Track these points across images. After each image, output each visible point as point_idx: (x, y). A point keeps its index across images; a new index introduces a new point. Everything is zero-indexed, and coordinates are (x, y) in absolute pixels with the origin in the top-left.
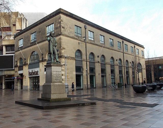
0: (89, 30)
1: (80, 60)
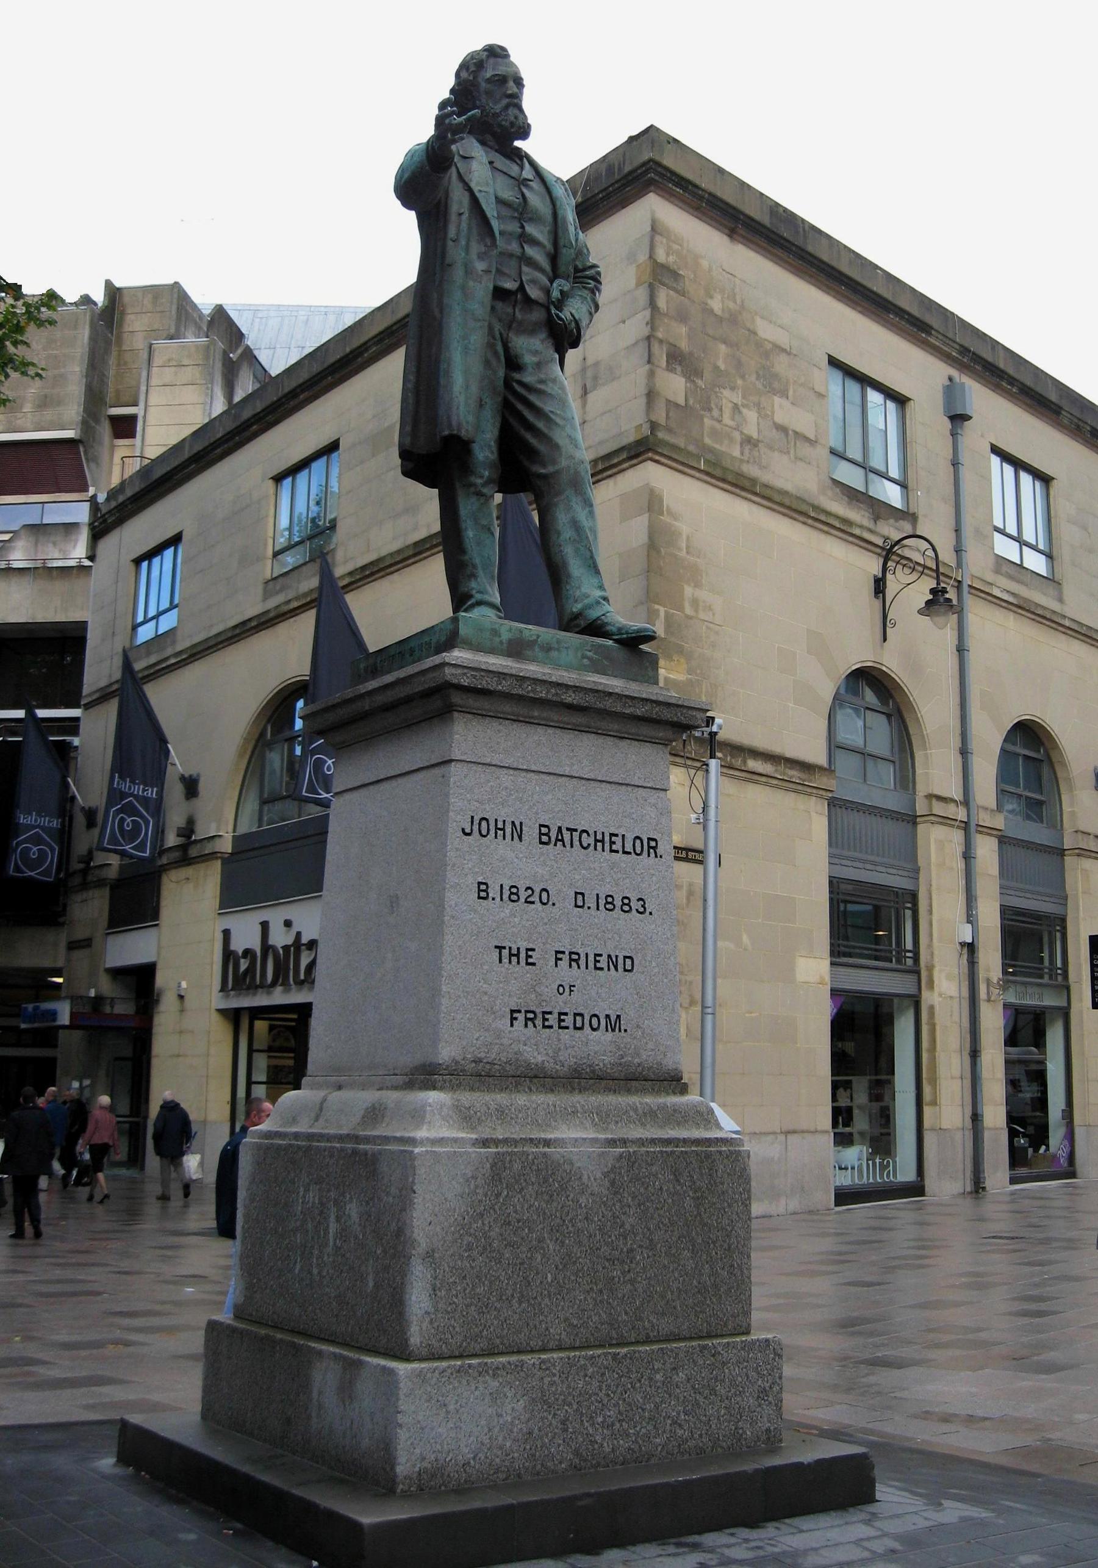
0: (995, 450)
1: (893, 802)
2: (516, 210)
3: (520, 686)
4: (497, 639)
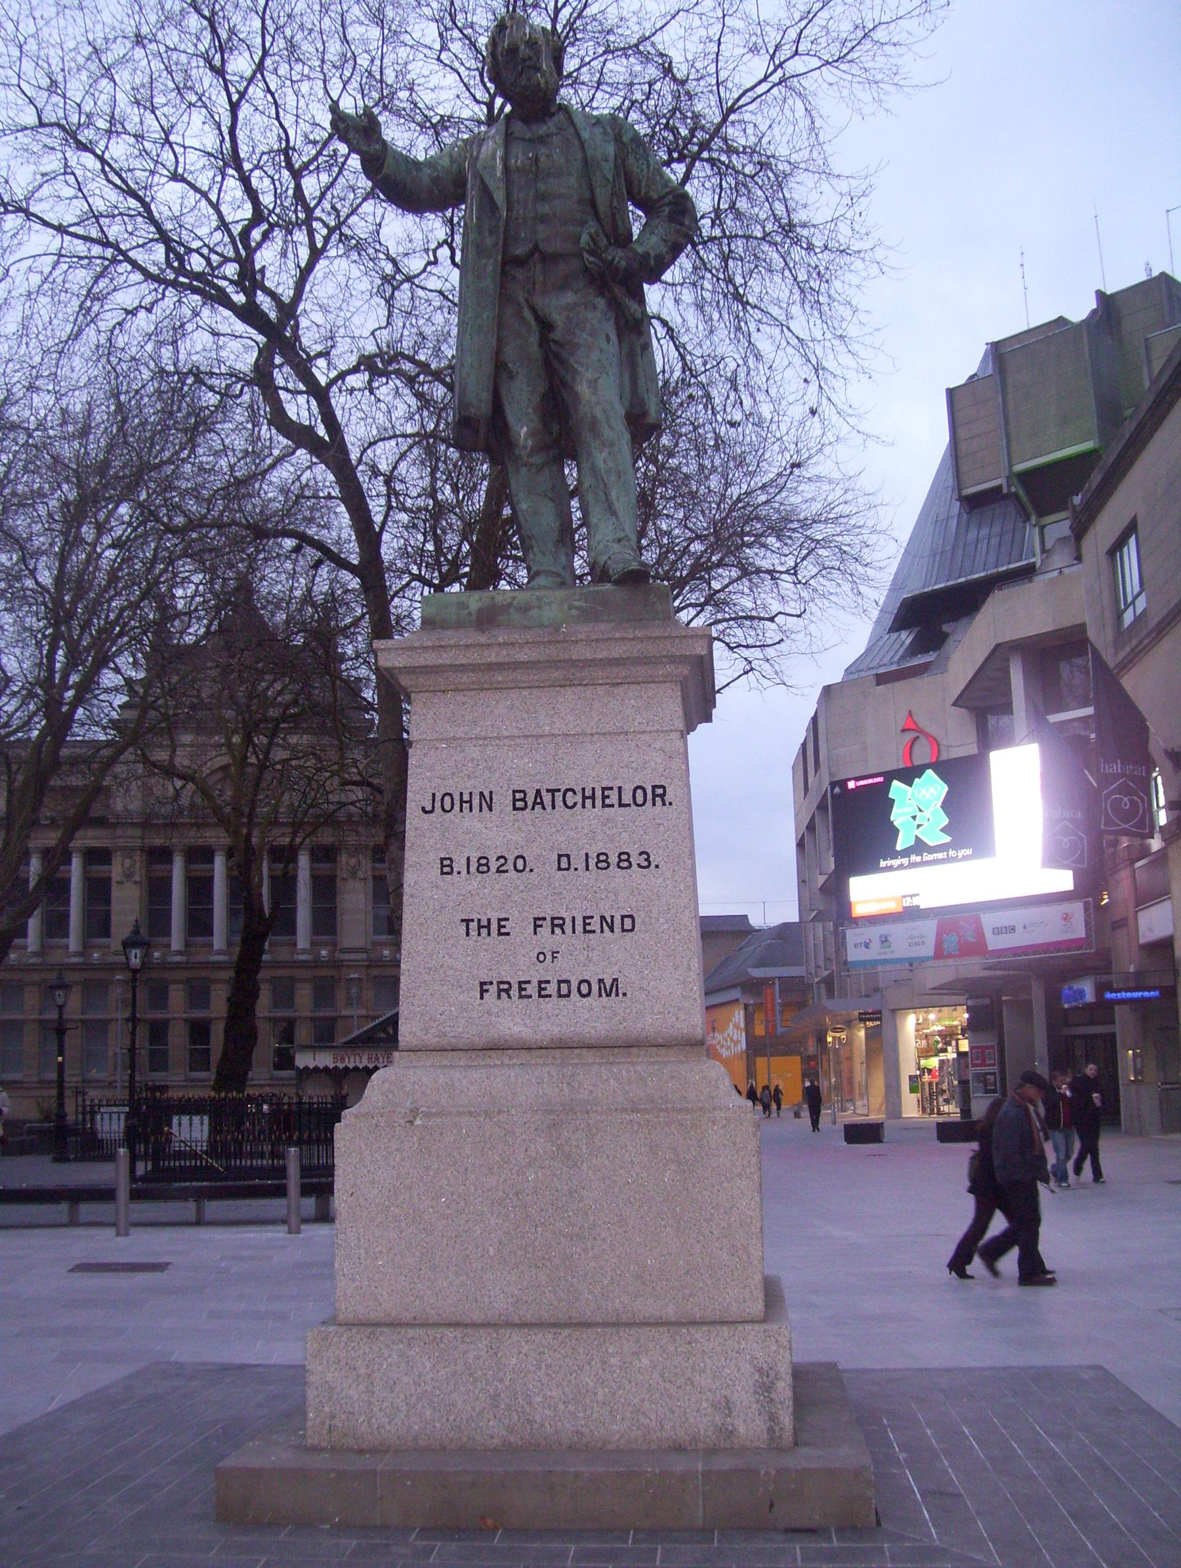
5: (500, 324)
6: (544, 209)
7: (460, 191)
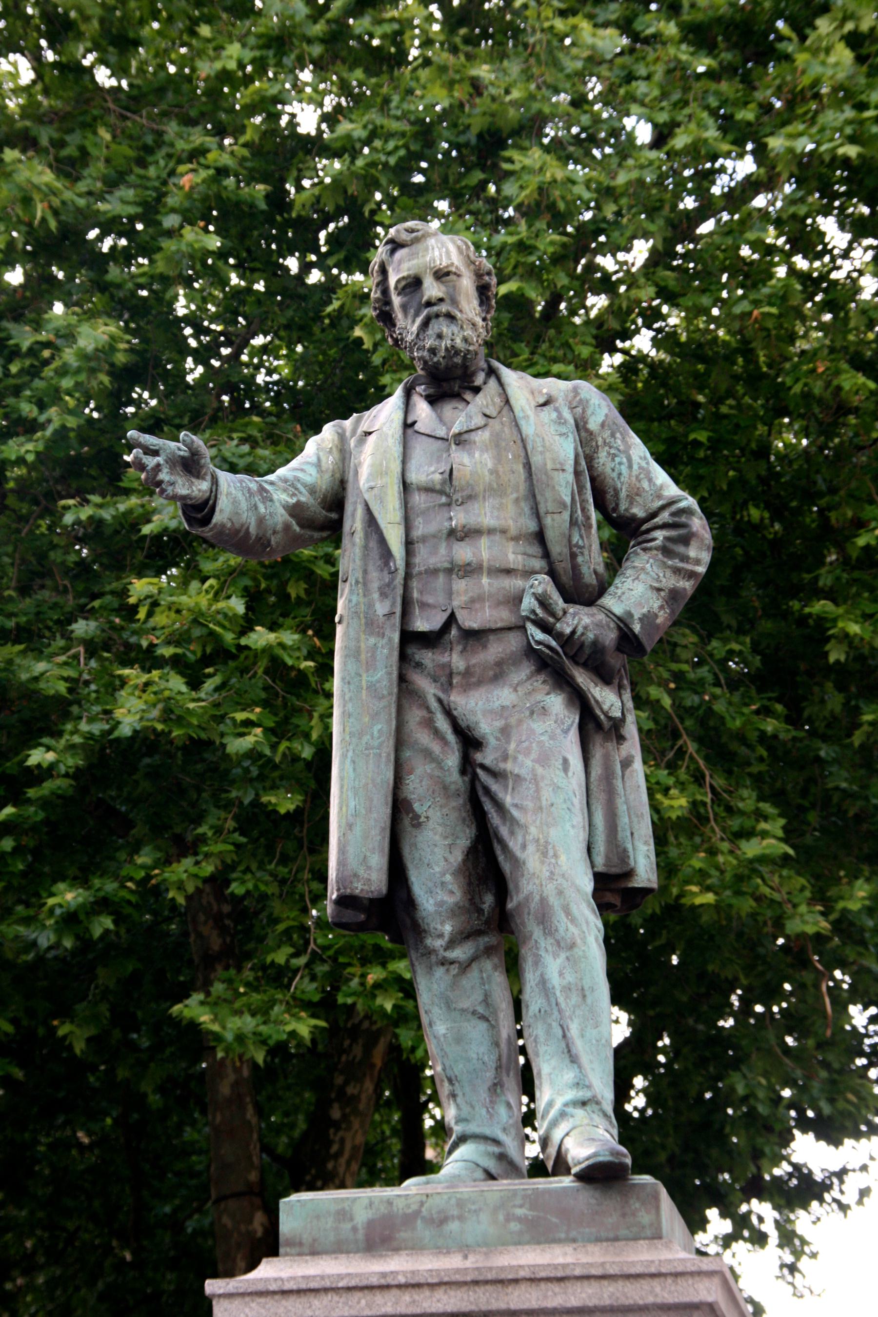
2: (441, 492)
3: (345, 1304)
4: (348, 1226)
5: (400, 741)
6: (464, 553)
7: (334, 516)
